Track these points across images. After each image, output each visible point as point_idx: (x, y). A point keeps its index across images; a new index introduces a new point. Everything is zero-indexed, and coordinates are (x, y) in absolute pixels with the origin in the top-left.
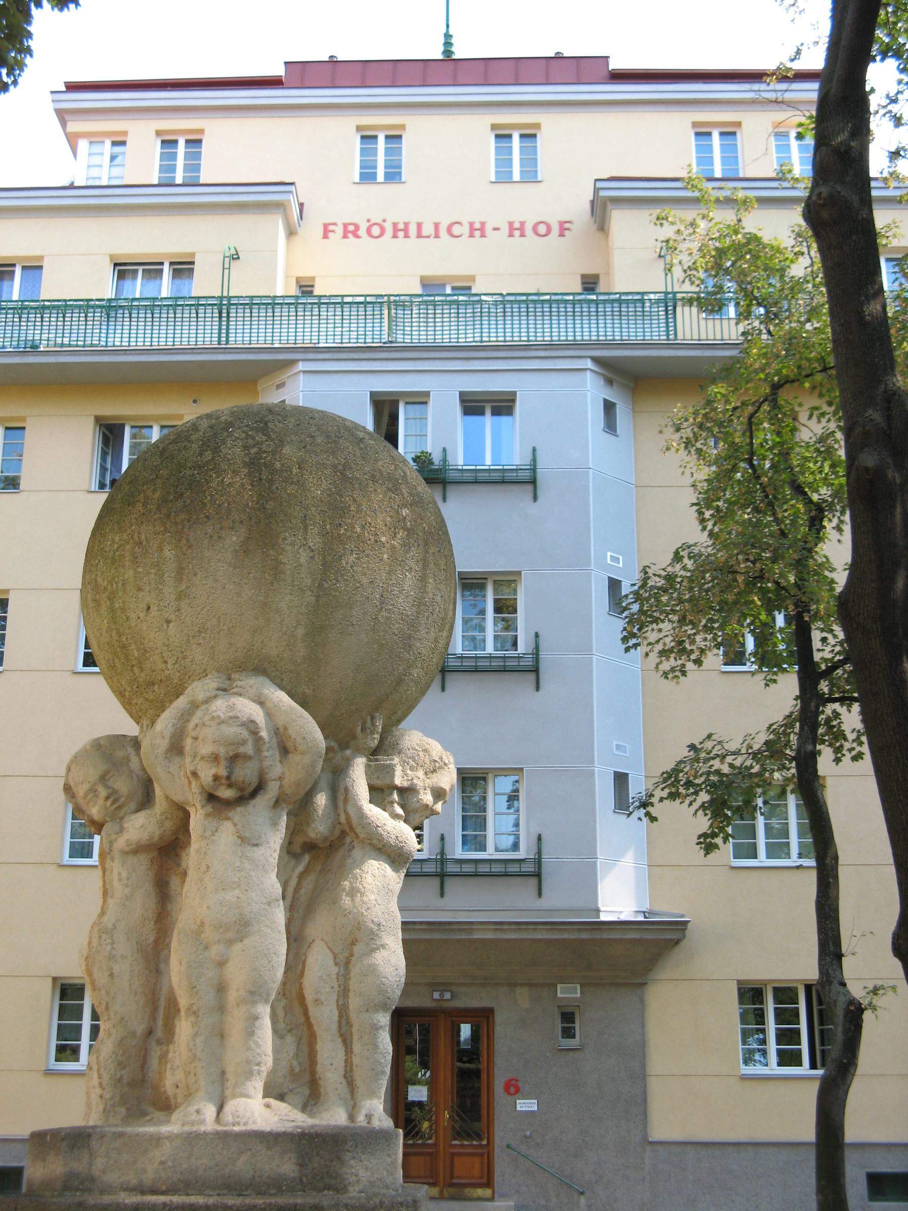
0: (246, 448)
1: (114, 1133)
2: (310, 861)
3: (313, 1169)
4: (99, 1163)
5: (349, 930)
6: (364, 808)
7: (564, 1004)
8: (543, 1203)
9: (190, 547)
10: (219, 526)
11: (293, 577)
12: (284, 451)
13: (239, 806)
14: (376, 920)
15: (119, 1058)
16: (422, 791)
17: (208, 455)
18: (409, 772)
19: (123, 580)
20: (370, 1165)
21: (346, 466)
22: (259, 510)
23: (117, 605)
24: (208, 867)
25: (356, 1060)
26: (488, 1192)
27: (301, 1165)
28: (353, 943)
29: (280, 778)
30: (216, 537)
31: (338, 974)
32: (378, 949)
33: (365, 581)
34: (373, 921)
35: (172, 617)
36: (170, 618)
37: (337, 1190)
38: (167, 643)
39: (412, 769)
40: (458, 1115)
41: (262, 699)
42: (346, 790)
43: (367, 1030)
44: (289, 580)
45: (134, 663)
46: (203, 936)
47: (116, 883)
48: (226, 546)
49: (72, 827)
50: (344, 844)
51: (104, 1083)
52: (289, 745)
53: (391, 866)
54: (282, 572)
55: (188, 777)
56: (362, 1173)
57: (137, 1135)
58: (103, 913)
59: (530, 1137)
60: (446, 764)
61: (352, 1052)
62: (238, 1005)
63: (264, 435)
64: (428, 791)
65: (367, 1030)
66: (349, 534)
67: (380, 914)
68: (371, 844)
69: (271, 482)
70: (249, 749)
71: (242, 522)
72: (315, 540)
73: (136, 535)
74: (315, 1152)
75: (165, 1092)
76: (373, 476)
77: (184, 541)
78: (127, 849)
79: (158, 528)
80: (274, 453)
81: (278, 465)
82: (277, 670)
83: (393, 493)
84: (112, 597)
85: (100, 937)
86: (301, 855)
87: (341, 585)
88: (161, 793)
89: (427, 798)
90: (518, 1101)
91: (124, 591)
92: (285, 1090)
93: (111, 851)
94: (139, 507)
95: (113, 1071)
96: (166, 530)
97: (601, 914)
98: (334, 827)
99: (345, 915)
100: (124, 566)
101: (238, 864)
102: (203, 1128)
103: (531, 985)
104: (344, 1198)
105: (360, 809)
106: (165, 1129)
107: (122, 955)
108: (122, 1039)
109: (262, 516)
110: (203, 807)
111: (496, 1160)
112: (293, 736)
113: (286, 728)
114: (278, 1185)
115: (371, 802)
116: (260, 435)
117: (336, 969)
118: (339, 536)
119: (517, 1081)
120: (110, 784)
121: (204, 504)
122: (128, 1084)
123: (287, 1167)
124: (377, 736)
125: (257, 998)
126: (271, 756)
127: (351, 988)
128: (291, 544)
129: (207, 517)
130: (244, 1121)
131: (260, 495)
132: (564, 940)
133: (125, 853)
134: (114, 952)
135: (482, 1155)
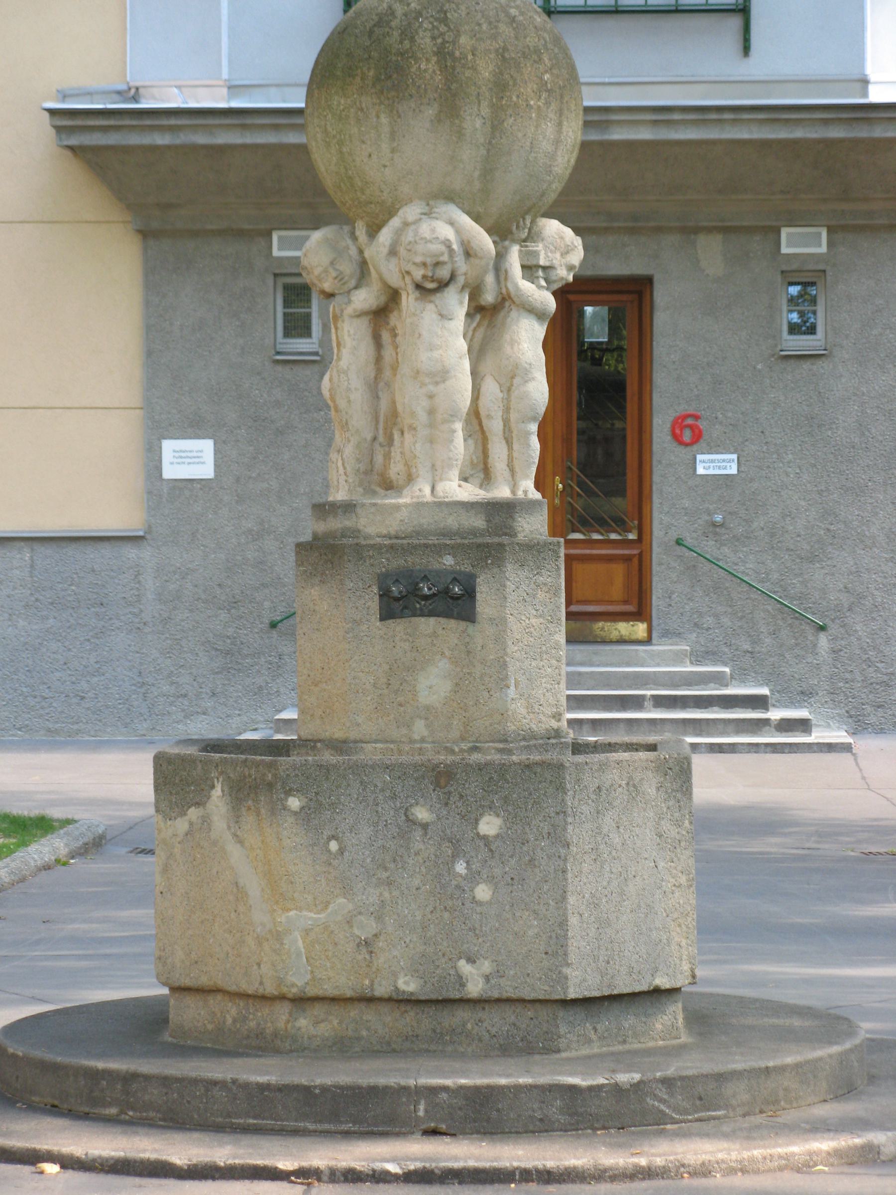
0: (434, 38)
1: (370, 504)
4: (363, 521)
6: (520, 284)
7: (795, 266)
8: (747, 646)
9: (399, 117)
10: (419, 102)
12: (461, 41)
14: (528, 361)
16: (559, 268)
18: (549, 254)
21: (505, 49)
22: (447, 90)
25: (515, 455)
26: (640, 629)
27: (488, 521)
28: (512, 378)
30: (417, 110)
32: (530, 380)
34: (526, 362)
35: (388, 164)
37: (511, 536)
39: (551, 252)
40: (581, 484)
42: (506, 271)
47: (346, 337)
52: (471, 252)
55: (402, 274)
56: (525, 526)
57: (385, 505)
59: (722, 525)
60: (576, 247)
61: (512, 449)
64: (564, 267)
66: (508, 103)
68: (524, 308)
69: (453, 68)
70: (445, 258)
72: (485, 111)
75: (389, 478)
76: (524, 53)
77: (395, 112)
81: (457, 54)
84: (341, 143)
85: (339, 376)
88: (377, 276)
90: (699, 457)
91: (351, 141)
92: (468, 475)
93: (342, 315)
94: (358, 80)
96: (381, 103)
97: (871, 88)
98: (498, 296)
99: (508, 359)
100: (350, 124)
102: (425, 500)
103: (726, 230)
104: (516, 540)
105: (516, 286)
106: (401, 501)
110: (413, 293)
111: (655, 568)
114: (474, 532)
116: (443, 26)
117: (501, 395)
118: (502, 106)
119: (697, 417)
120: (337, 267)
121: (408, 85)
122: (363, 472)
123: (479, 522)
124: (527, 230)
125: (455, 419)
126: (460, 260)
129: (411, 95)
132: (795, 142)
133: (352, 317)
135: (627, 559)
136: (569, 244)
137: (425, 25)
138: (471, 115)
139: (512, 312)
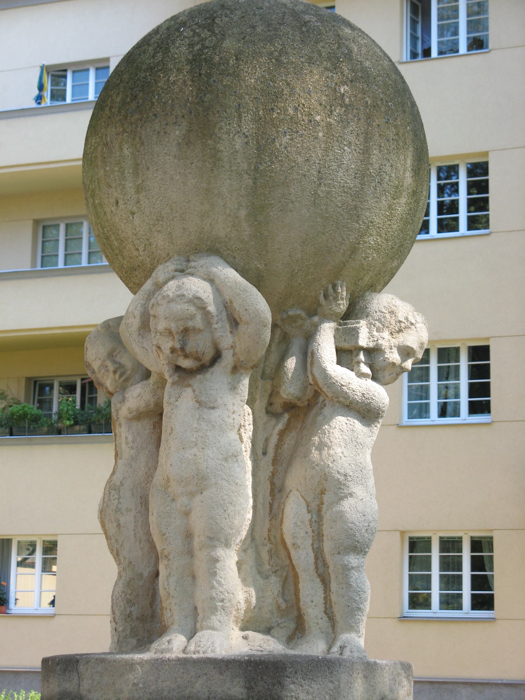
2: (289, 420)
3: (259, 692)
4: (86, 684)
5: (317, 481)
10: (165, 122)
11: (230, 162)
12: (224, 45)
13: (199, 374)
14: (342, 471)
15: (128, 596)
16: (387, 351)
17: (160, 56)
18: (375, 333)
19: (98, 179)
20: (311, 690)
23: (97, 202)
24: (172, 430)
25: (334, 598)
28: (322, 492)
29: (232, 347)
30: (162, 133)
31: (310, 521)
33: (300, 160)
34: (339, 472)
35: (135, 209)
36: (133, 210)
38: (135, 232)
39: (378, 330)
41: (212, 277)
42: (313, 353)
43: (340, 571)
44: (227, 167)
45: (117, 251)
46: (170, 489)
48: (171, 140)
49: (439, 389)
50: (318, 403)
51: (117, 618)
53: (361, 422)
54: (220, 159)
57: (115, 661)
58: (114, 473)
60: (412, 324)
62: (200, 549)
63: (209, 30)
64: (395, 350)
65: (340, 571)
66: (282, 117)
67: (346, 465)
68: (339, 402)
69: (209, 75)
70: (198, 322)
71: (183, 116)
73: (104, 137)
74: (259, 678)
77: (137, 139)
78: (130, 416)
79: (118, 129)
80: (214, 48)
81: (217, 59)
82: (229, 249)
83: (331, 71)
85: (110, 493)
86: (281, 414)
87: (276, 166)
89: (394, 357)
95: (122, 608)
96: (124, 131)
99: (313, 468)
100: (97, 167)
101: (195, 425)
102: (168, 655)
107: (127, 508)
108: (129, 582)
109: (201, 109)
112: (237, 309)
113: (231, 302)
115: (339, 363)
117: (309, 516)
118: (272, 120)
120: (117, 359)
121: (153, 103)
122: (137, 618)
125: (216, 543)
127: (324, 533)
128: (226, 133)
129: (155, 115)
130: (203, 650)
131: (199, 89)
133: (130, 420)
134: (120, 506)
136: (402, 319)
137: (185, 34)
138: (228, 133)
139: (325, 408)
